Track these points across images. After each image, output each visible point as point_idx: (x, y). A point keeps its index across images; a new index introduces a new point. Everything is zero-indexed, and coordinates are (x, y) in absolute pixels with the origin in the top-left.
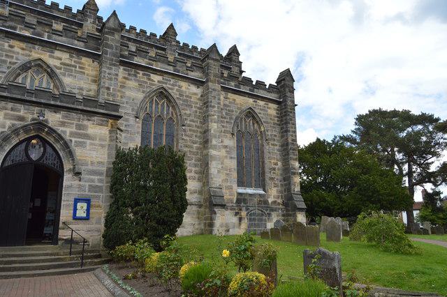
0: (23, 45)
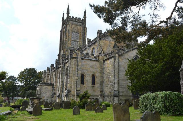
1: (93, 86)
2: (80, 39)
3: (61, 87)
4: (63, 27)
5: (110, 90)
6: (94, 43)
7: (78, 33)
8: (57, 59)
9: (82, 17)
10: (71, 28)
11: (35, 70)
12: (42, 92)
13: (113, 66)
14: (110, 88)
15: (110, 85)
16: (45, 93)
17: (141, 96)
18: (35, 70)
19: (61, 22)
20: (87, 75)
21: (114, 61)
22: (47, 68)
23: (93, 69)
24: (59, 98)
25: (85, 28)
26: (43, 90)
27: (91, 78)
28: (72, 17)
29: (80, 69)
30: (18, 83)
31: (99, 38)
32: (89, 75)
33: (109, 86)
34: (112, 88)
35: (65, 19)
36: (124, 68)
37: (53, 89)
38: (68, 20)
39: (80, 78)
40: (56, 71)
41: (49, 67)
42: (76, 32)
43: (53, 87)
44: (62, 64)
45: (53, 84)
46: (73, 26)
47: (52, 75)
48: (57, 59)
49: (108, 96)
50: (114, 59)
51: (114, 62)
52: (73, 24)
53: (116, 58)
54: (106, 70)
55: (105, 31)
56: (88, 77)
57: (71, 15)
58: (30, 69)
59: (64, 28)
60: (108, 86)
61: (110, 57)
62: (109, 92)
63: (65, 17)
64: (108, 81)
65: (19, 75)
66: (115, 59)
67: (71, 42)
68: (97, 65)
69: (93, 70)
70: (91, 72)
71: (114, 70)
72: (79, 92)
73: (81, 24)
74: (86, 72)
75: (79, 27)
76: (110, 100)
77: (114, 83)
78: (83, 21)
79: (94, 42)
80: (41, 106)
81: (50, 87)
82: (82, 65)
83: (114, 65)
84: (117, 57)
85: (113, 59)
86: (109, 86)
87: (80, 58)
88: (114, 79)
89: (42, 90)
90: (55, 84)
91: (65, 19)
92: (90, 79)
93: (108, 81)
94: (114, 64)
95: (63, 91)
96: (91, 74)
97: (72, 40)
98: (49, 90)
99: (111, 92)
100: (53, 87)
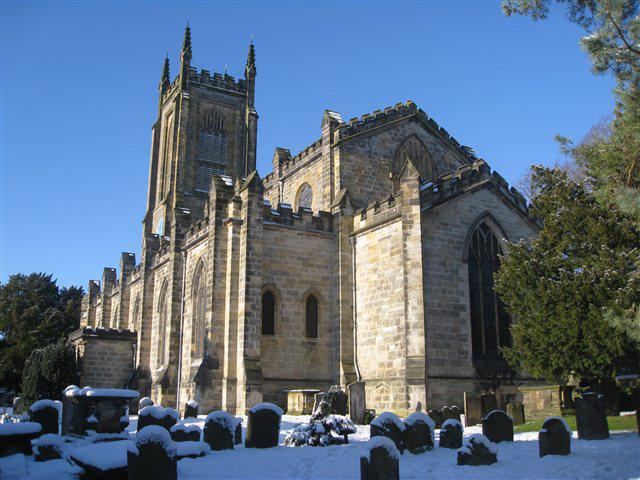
1: (312, 340)
2: (233, 156)
3: (171, 348)
4: (164, 112)
5: (384, 357)
6: (307, 164)
7: (224, 133)
10: (198, 112)
11: (52, 281)
13: (398, 258)
14: (382, 348)
15: (383, 334)
17: (332, 416)
18: (52, 281)
20: (285, 296)
21: (406, 236)
22: (106, 269)
23: (309, 269)
24: (163, 392)
26: (94, 358)
27: (303, 310)
29: (259, 268)
31: (332, 141)
32: (296, 294)
33: (379, 338)
34: (392, 347)
36: (444, 264)
39: (260, 306)
40: (146, 278)
41: (117, 265)
44: (178, 250)
45: (136, 334)
47: (129, 300)
49: (375, 381)
50: (404, 228)
51: (405, 239)
53: (412, 222)
54: (363, 275)
55: (610, 80)
56: (288, 304)
57: (198, 64)
58: (34, 276)
60: (372, 342)
61: (379, 217)
62: (382, 365)
63: (176, 70)
64: (376, 318)
66: (407, 224)
67: (195, 168)
68: (323, 253)
69: (311, 275)
70: (302, 282)
71: (406, 273)
72: (258, 364)
74: (280, 283)
76: (387, 398)
77: (407, 327)
78: (243, 90)
79: (306, 160)
80: (623, 354)
82: (266, 254)
83: (405, 252)
84: (417, 221)
85: (399, 225)
86: (379, 338)
87: (259, 221)
88: (406, 310)
90: (142, 333)
92: (297, 314)
93: (376, 318)
94: (405, 246)
95: (175, 362)
96: (303, 290)
97: (201, 164)
99: (390, 365)
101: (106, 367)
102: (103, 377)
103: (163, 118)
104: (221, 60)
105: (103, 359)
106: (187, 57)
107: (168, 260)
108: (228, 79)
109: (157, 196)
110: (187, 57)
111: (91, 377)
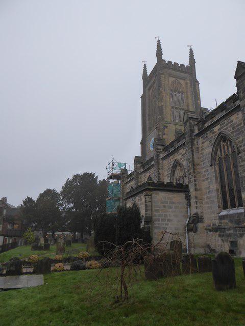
0: (172, 157)
8: (139, 155)
9: (186, 63)
12: (170, 210)
16: (166, 216)
19: (142, 81)
25: (195, 83)
28: (167, 62)
30: (62, 205)
35: (148, 74)
37: (189, 204)
38: (161, 67)
42: (179, 92)
43: (188, 198)
46: (172, 79)
48: (139, 155)
52: (170, 75)
57: (166, 57)
58: (85, 174)
59: (149, 89)
65: (63, 188)
73: (186, 75)
75: (182, 82)
78: (190, 70)
81: (179, 198)
89: (154, 208)
91: (148, 74)
97: (173, 108)
98: (176, 207)
100: (188, 198)
101: (168, 214)
102: (166, 222)
103: (147, 91)
104: (176, 55)
105: (165, 207)
106: (159, 53)
107: (133, 178)
108: (183, 65)
109: (147, 129)
110: (159, 53)
111: (157, 222)
